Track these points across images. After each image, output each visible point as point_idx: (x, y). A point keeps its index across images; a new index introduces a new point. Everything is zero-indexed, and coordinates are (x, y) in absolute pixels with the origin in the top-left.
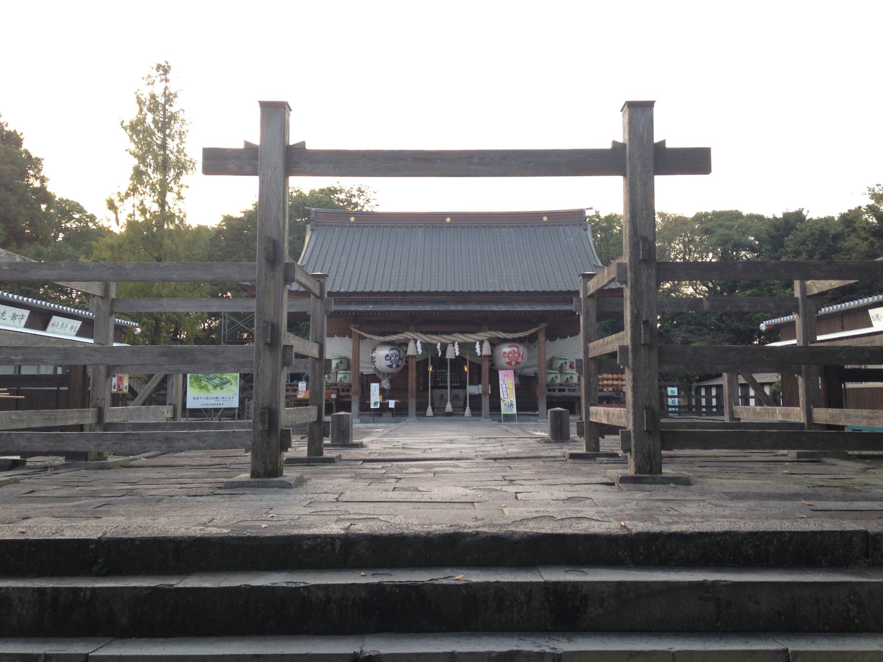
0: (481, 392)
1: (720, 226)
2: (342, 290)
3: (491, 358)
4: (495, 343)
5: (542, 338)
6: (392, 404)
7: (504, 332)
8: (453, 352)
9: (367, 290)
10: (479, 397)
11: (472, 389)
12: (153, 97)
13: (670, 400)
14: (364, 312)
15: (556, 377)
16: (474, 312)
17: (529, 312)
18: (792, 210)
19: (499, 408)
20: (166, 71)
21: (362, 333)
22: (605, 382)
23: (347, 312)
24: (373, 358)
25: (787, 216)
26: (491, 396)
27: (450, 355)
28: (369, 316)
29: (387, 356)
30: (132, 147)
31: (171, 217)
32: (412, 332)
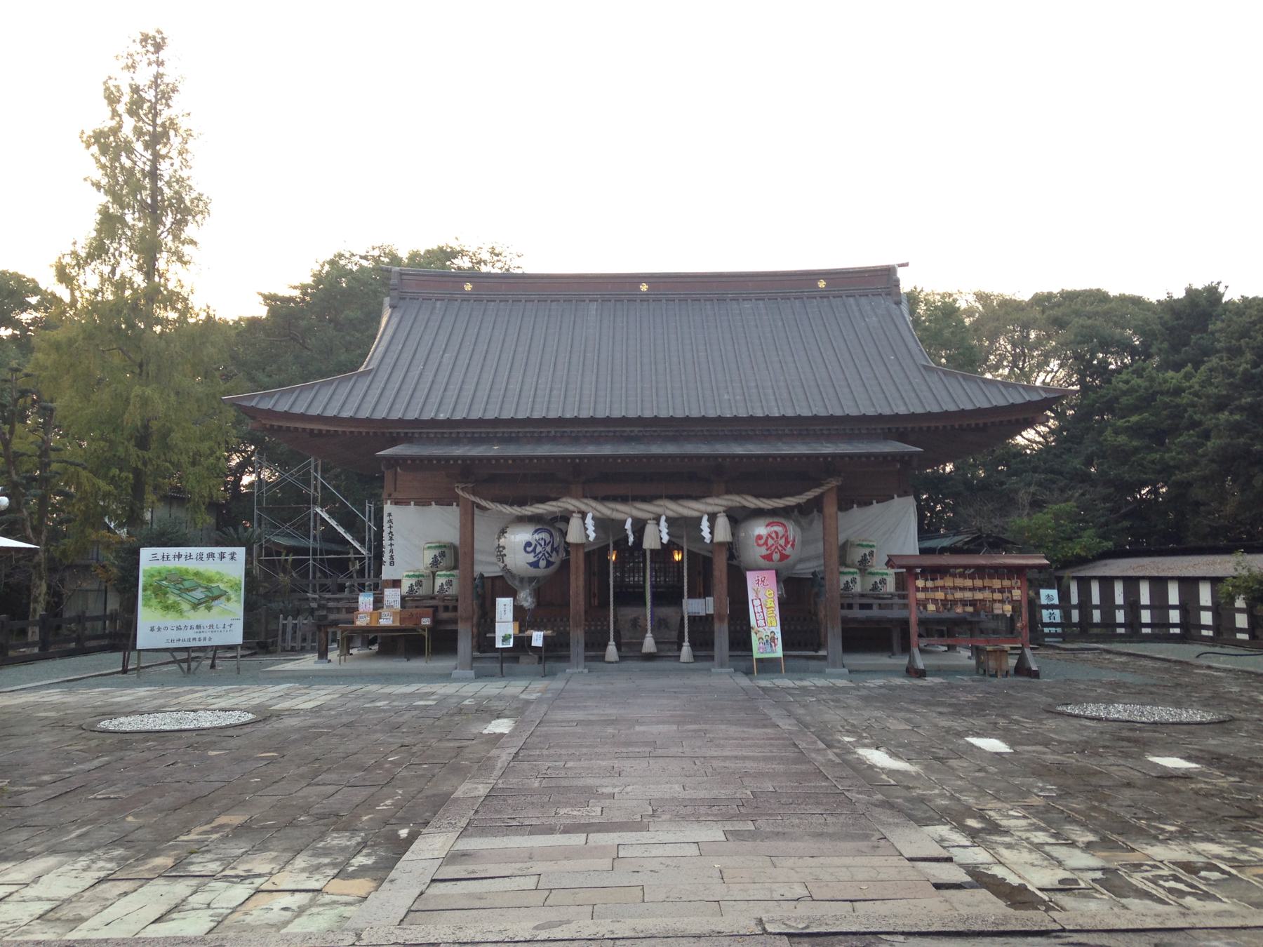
0: (711, 611)
1: (1077, 313)
2: (442, 416)
3: (731, 549)
4: (737, 518)
5: (830, 507)
6: (537, 638)
7: (757, 496)
8: (655, 536)
9: (490, 415)
10: (708, 619)
11: (694, 606)
12: (136, 90)
13: (1045, 613)
14: (481, 459)
15: (854, 581)
16: (699, 457)
17: (808, 456)
18: (1199, 285)
19: (748, 646)
20: (158, 47)
21: (478, 500)
22: (959, 595)
23: (447, 459)
24: (500, 548)
25: (1190, 292)
26: (732, 618)
27: (650, 543)
28: (493, 467)
29: (528, 544)
30: (98, 175)
31: (172, 299)
32: (576, 497)
